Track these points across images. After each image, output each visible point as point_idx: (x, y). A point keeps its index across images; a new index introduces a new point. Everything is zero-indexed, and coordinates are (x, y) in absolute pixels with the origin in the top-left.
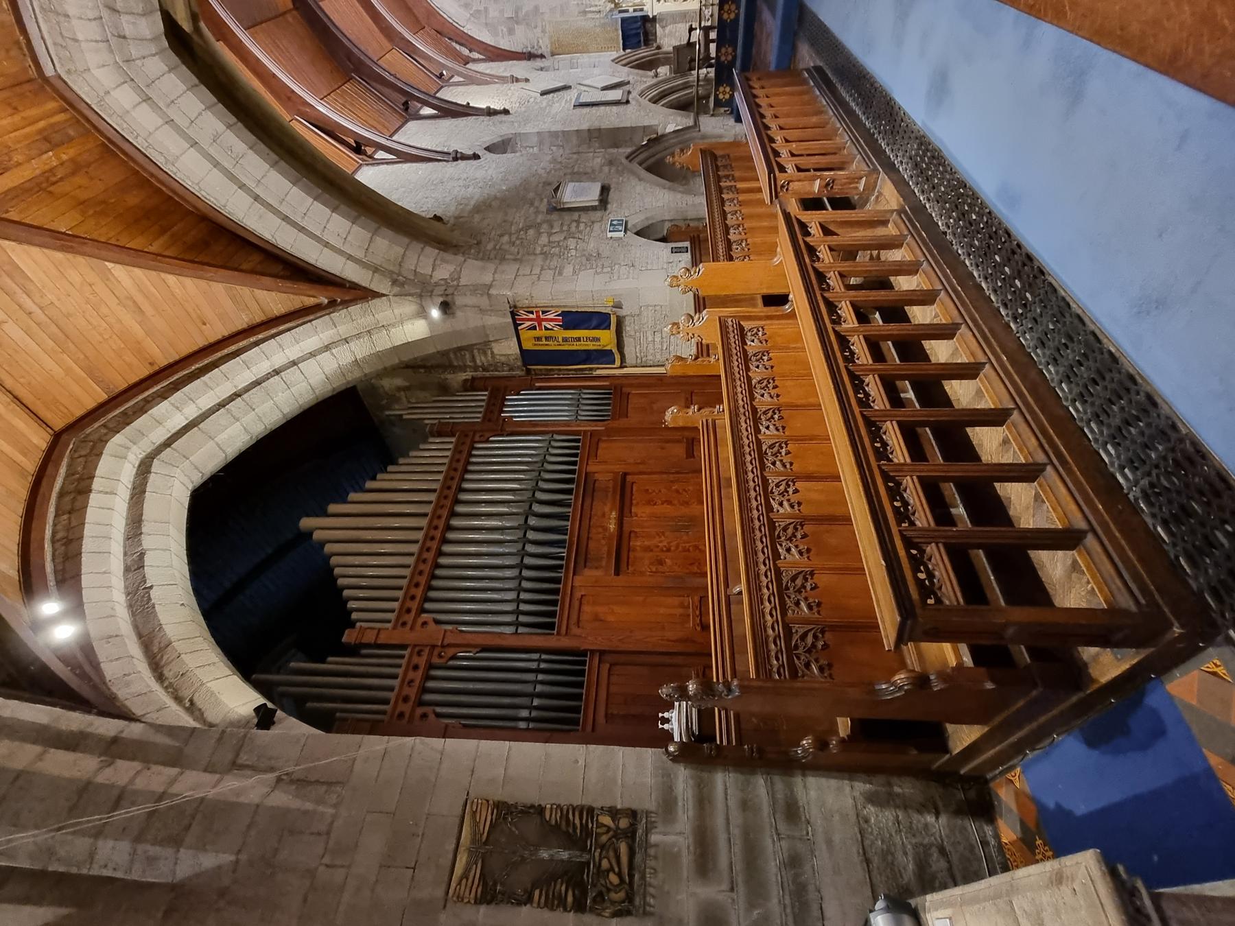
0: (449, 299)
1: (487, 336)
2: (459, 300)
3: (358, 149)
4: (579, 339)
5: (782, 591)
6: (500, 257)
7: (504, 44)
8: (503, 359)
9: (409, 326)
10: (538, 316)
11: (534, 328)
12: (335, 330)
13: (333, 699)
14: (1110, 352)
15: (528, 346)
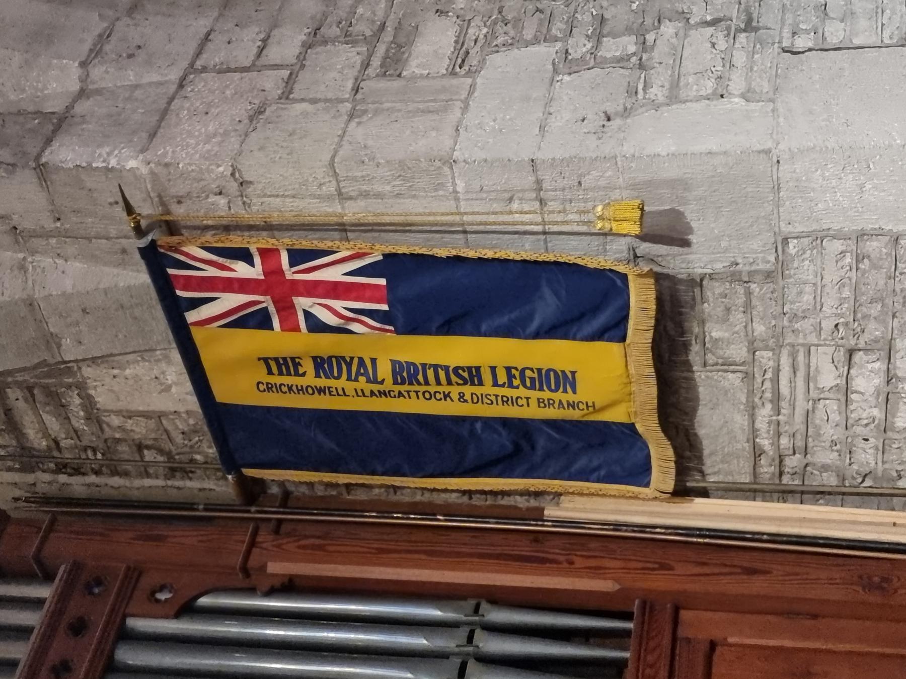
4: (473, 376)
10: (273, 272)
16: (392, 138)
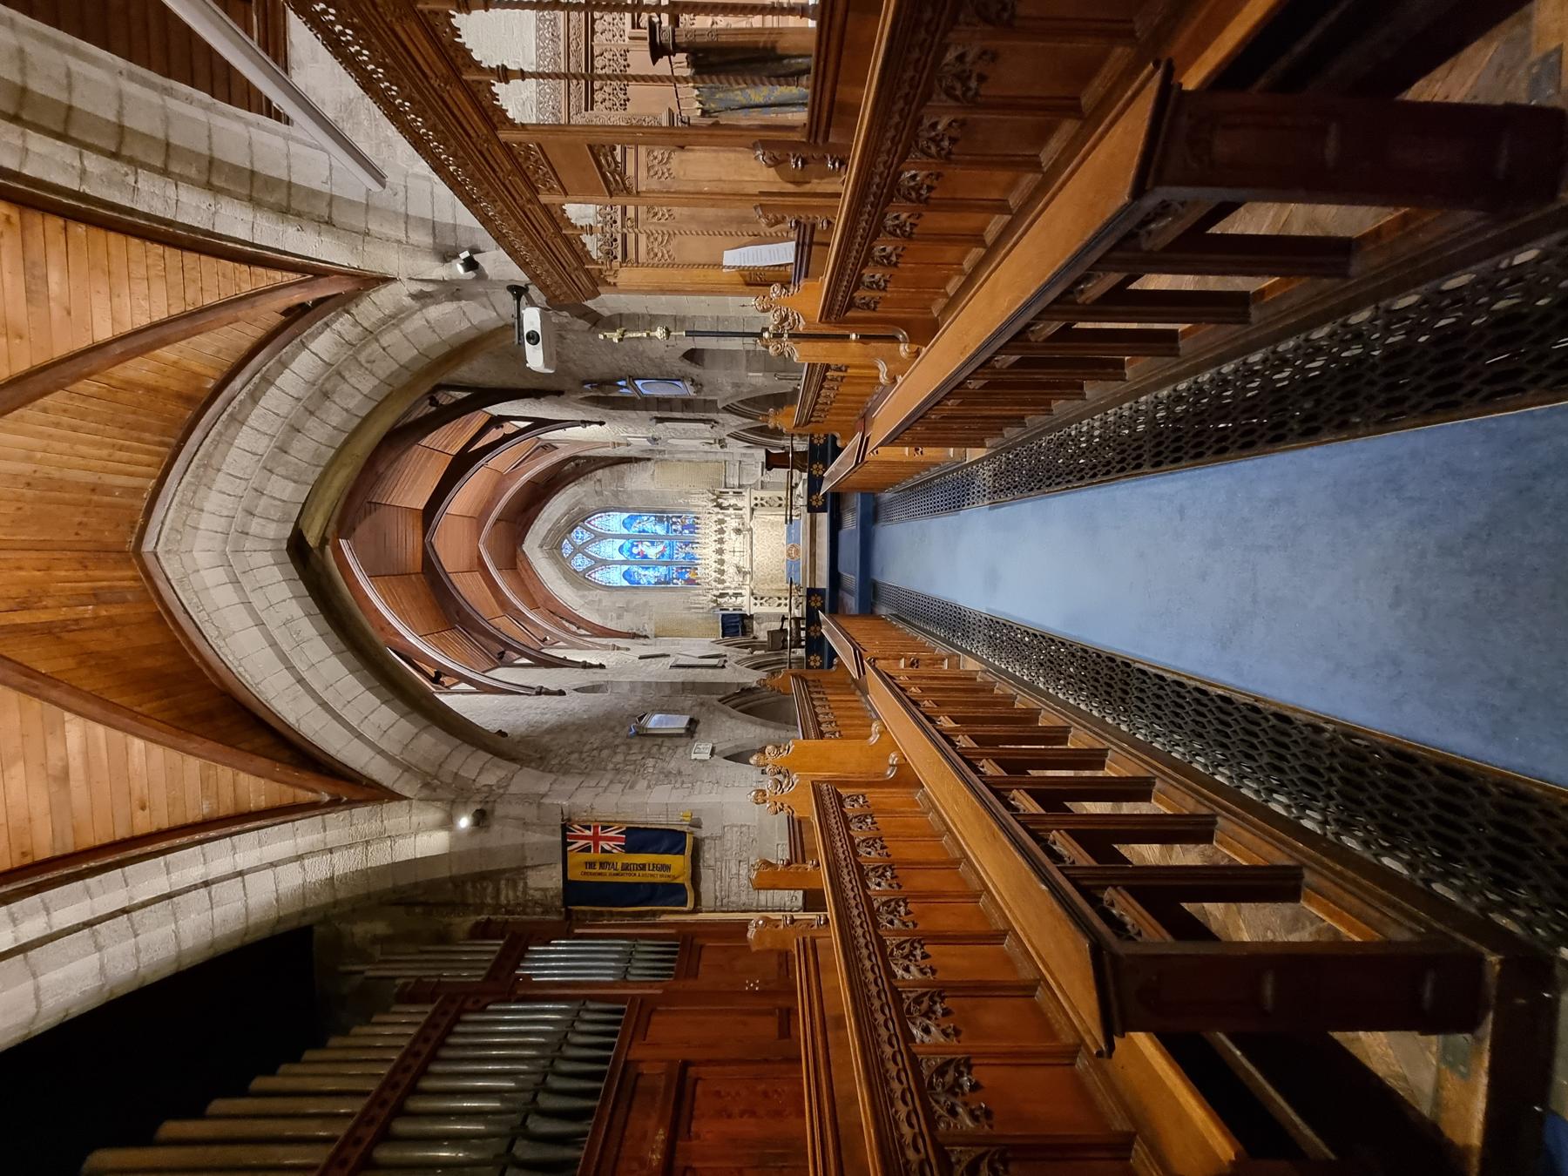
0: (488, 807)
1: (525, 858)
2: (500, 810)
3: (435, 680)
4: (643, 867)
5: (925, 1091)
6: (565, 770)
7: (611, 625)
8: (538, 895)
9: (421, 837)
10: (596, 833)
11: (587, 849)
12: (319, 836)
14: (1219, 696)
15: (575, 875)
16: (631, 799)
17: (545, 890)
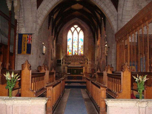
4: (25, 47)
10: (30, 39)
11: (28, 38)
13: (134, 73)
15: (24, 36)
17: (21, 30)
